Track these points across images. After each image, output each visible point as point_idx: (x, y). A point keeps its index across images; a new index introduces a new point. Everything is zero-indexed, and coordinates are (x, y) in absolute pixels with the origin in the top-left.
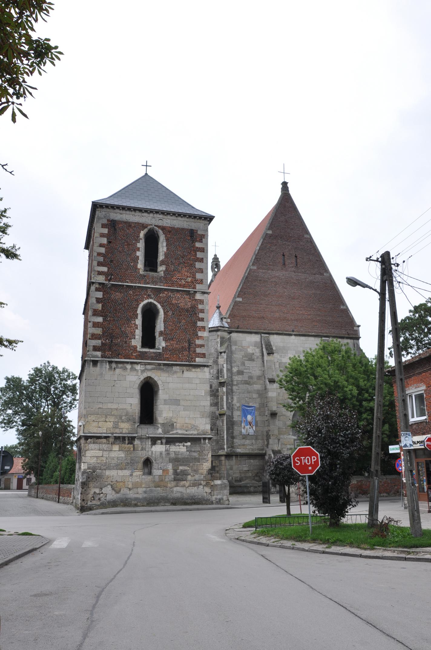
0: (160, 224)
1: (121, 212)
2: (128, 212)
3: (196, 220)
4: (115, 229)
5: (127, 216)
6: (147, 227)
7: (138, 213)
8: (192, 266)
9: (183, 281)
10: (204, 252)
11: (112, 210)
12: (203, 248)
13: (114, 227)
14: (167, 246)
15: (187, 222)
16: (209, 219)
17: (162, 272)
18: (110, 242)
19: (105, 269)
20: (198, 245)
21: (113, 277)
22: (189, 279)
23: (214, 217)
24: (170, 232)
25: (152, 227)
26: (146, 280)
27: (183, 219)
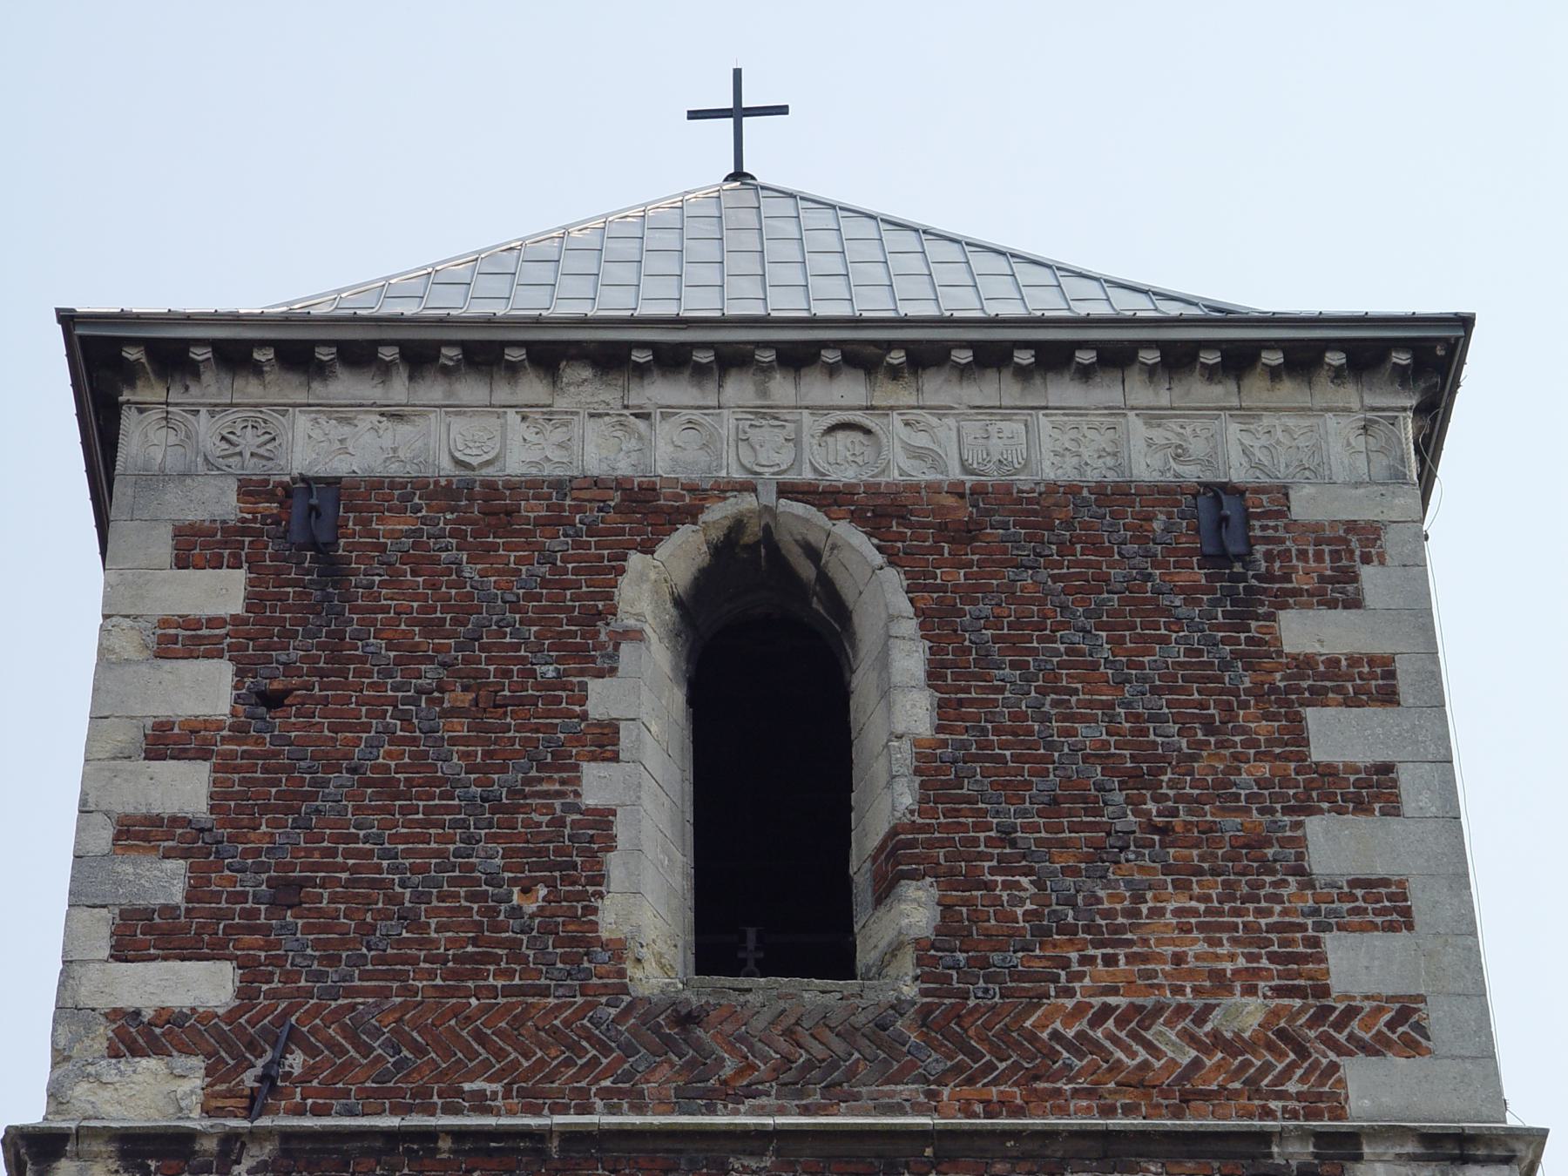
0: (845, 475)
1: (399, 390)
2: (471, 390)
3: (1257, 390)
4: (333, 569)
5: (459, 425)
6: (690, 514)
7: (582, 389)
8: (1265, 857)
9: (1164, 1034)
10: (1389, 697)
11: (283, 388)
12: (1384, 667)
13: (323, 550)
14: (934, 675)
15: (1154, 417)
16: (1418, 362)
17: (907, 964)
18: (272, 700)
19: (207, 985)
20: (1304, 632)
21: (296, 1061)
22: (1247, 1013)
23: (58, 311)
24: (965, 534)
25: (748, 502)
26: (700, 1065)
27: (1105, 392)
